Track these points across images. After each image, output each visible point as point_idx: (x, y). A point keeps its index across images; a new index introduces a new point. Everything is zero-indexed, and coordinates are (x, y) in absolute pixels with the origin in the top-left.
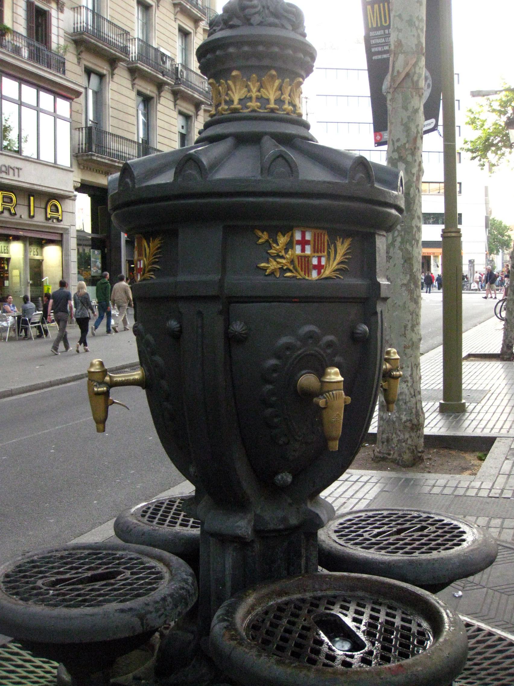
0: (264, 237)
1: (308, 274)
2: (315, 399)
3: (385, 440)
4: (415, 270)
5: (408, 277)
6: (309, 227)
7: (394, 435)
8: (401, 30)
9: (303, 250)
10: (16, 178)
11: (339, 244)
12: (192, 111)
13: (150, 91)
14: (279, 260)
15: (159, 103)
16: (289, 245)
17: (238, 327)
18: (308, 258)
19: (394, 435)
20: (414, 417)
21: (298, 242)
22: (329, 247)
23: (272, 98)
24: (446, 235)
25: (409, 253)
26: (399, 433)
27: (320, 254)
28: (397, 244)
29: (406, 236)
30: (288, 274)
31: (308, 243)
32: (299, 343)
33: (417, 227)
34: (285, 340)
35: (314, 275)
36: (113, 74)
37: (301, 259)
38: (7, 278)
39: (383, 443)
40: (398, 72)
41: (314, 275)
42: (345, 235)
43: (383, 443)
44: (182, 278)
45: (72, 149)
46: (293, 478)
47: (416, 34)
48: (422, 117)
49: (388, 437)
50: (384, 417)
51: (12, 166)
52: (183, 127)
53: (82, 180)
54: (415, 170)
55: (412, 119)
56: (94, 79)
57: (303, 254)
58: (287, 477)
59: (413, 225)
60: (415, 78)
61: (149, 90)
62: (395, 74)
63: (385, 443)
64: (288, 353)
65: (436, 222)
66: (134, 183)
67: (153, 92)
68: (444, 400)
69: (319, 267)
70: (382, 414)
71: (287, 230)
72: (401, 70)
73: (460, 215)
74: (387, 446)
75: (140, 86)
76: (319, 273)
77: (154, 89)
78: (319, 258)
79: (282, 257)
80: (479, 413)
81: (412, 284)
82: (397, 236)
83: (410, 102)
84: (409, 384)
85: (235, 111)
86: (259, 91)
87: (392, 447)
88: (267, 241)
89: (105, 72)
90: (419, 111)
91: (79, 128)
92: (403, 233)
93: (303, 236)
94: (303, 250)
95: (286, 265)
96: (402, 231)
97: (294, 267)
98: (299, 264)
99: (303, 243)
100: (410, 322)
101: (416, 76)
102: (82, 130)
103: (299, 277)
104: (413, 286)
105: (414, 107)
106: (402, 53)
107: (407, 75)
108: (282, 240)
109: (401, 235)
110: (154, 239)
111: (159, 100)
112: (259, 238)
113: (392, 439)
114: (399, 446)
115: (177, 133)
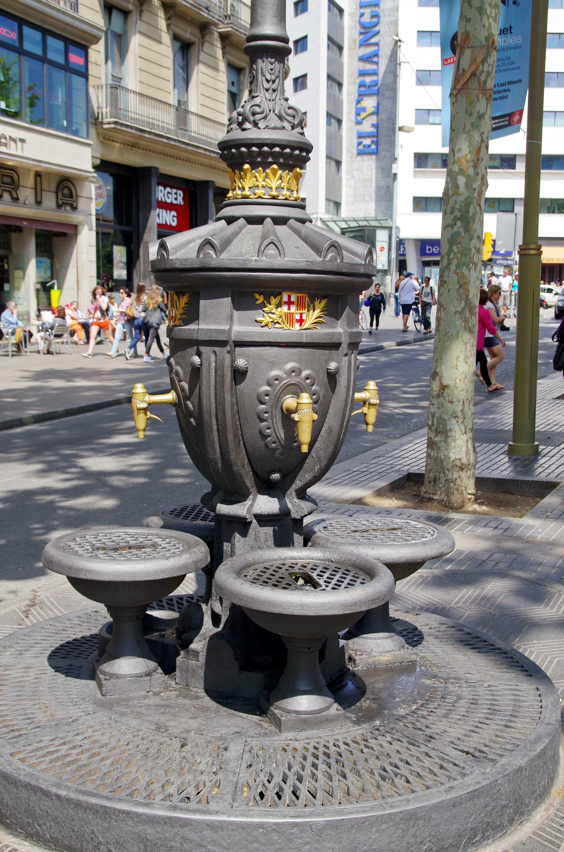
0: (261, 299)
2: (292, 415)
3: (432, 480)
4: (470, 296)
5: (463, 303)
7: (442, 475)
8: (470, 19)
9: (289, 309)
10: (19, 153)
11: (317, 303)
12: (245, 62)
13: (191, 34)
14: (271, 315)
15: (202, 51)
19: (442, 475)
20: (464, 455)
21: (285, 303)
22: (309, 306)
23: (274, 187)
24: (523, 252)
25: (465, 277)
26: (447, 473)
27: (301, 311)
28: (453, 267)
29: (463, 258)
30: (278, 326)
31: (293, 303)
32: (285, 376)
33: (475, 248)
34: (275, 373)
36: (141, 12)
38: (8, 281)
39: (430, 482)
40: (463, 70)
42: (322, 298)
43: (430, 482)
44: (202, 326)
47: (487, 25)
49: (435, 476)
50: (432, 455)
51: (14, 137)
52: (233, 83)
53: (102, 155)
54: (476, 185)
55: (477, 126)
56: (117, 17)
57: (289, 311)
58: (276, 476)
59: (472, 247)
60: (483, 78)
61: (188, 33)
62: (460, 72)
63: (432, 483)
64: (277, 382)
66: (168, 256)
67: (195, 36)
68: (513, 442)
69: (301, 321)
70: (430, 451)
72: (466, 69)
74: (434, 485)
75: (178, 27)
76: (301, 325)
77: (197, 32)
79: (273, 313)
80: (553, 456)
81: (467, 311)
82: (453, 258)
83: (475, 106)
84: (460, 421)
85: (246, 197)
86: (264, 180)
87: (439, 487)
88: (263, 302)
89: (131, 7)
90: (486, 116)
91: (98, 86)
92: (459, 255)
93: (289, 297)
94: (289, 309)
96: (458, 252)
97: (282, 321)
100: (463, 352)
101: (484, 74)
102: (102, 88)
103: (285, 328)
104: (468, 314)
105: (479, 112)
106: (469, 48)
107: (473, 74)
109: (457, 258)
110: (183, 295)
111: (202, 46)
112: (257, 300)
113: (439, 479)
114: (446, 486)
115: (226, 92)
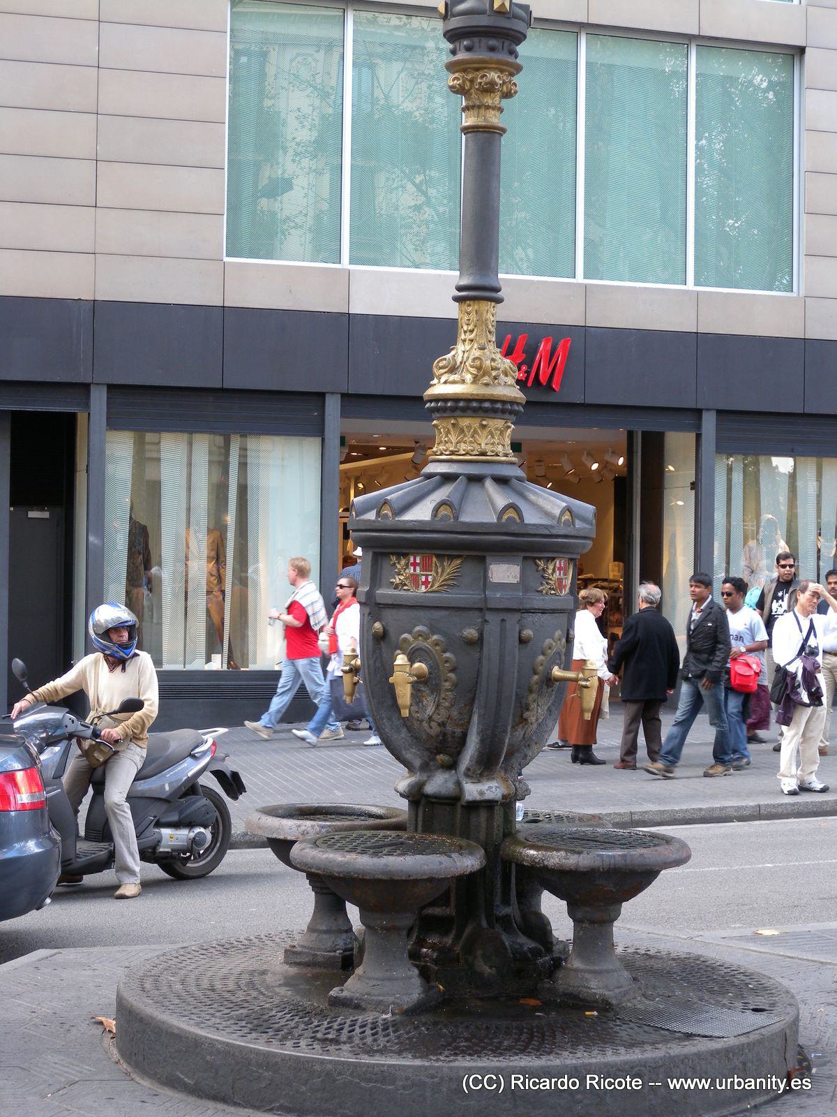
6: (418, 554)
9: (415, 570)
16: (407, 565)
17: (528, 632)
18: (417, 576)
31: (418, 564)
35: (423, 589)
42: (451, 558)
45: (487, 51)
46: (546, 639)
48: (284, 674)
69: (426, 583)
71: (406, 555)
73: (531, 12)
76: (426, 588)
78: (427, 576)
93: (415, 559)
94: (415, 570)
99: (415, 564)
108: (403, 562)
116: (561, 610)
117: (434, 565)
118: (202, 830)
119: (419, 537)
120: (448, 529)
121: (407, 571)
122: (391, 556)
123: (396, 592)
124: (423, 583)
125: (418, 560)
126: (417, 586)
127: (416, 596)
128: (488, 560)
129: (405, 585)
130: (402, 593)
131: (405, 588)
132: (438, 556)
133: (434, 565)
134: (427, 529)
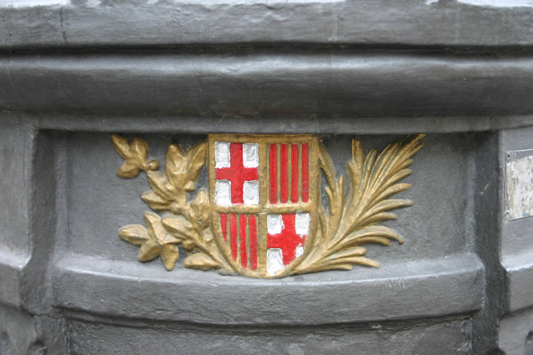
1: (254, 260)
6: (252, 137)
9: (237, 195)
16: (203, 177)
18: (252, 219)
35: (274, 263)
37: (243, 223)
41: (274, 263)
42: (377, 145)
65: (240, 189)
69: (287, 242)
78: (289, 218)
94: (237, 195)
95: (189, 238)
98: (225, 233)
99: (238, 175)
116: (266, 136)
117: (313, 174)
118: (30, 25)
119: (288, 74)
120: (417, 38)
121: (202, 198)
122: (124, 148)
123: (153, 274)
124: (274, 242)
125: (251, 158)
126: (252, 257)
127: (255, 291)
128: (507, 142)
129: (195, 248)
130: (179, 277)
131: (198, 259)
132: (328, 142)
133: (313, 174)
134: (334, 38)
